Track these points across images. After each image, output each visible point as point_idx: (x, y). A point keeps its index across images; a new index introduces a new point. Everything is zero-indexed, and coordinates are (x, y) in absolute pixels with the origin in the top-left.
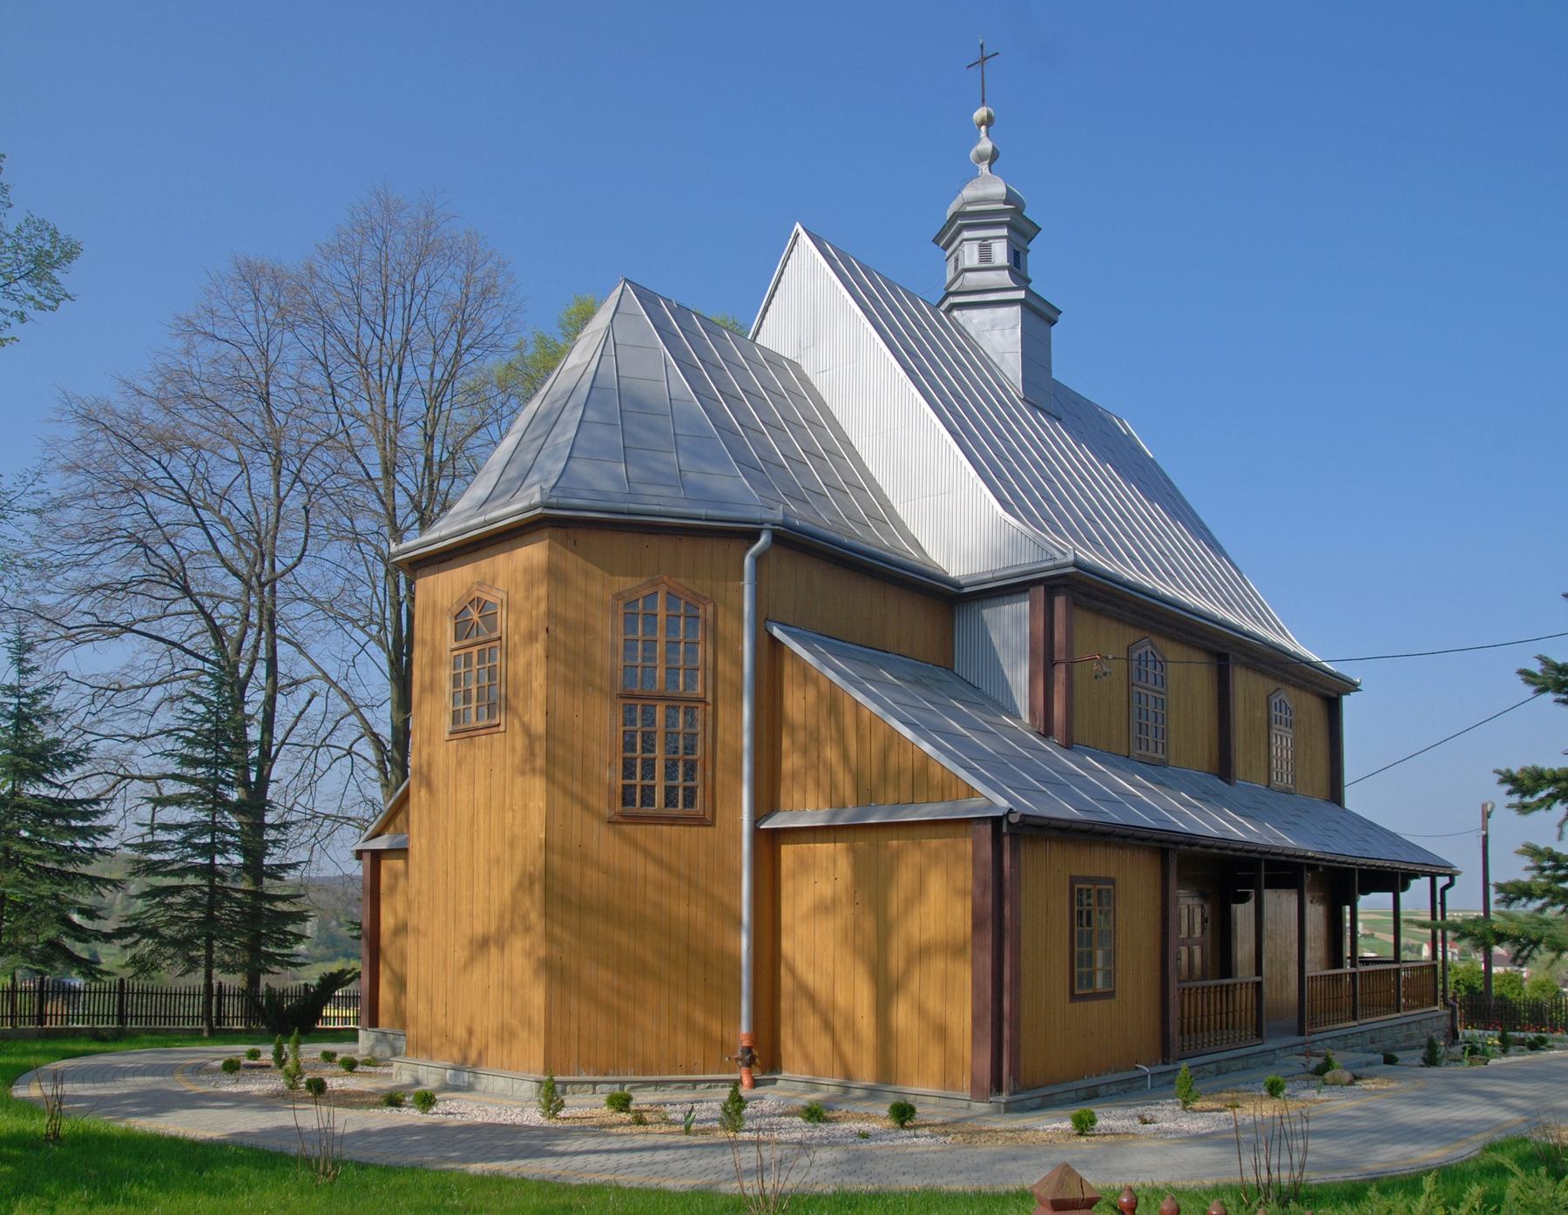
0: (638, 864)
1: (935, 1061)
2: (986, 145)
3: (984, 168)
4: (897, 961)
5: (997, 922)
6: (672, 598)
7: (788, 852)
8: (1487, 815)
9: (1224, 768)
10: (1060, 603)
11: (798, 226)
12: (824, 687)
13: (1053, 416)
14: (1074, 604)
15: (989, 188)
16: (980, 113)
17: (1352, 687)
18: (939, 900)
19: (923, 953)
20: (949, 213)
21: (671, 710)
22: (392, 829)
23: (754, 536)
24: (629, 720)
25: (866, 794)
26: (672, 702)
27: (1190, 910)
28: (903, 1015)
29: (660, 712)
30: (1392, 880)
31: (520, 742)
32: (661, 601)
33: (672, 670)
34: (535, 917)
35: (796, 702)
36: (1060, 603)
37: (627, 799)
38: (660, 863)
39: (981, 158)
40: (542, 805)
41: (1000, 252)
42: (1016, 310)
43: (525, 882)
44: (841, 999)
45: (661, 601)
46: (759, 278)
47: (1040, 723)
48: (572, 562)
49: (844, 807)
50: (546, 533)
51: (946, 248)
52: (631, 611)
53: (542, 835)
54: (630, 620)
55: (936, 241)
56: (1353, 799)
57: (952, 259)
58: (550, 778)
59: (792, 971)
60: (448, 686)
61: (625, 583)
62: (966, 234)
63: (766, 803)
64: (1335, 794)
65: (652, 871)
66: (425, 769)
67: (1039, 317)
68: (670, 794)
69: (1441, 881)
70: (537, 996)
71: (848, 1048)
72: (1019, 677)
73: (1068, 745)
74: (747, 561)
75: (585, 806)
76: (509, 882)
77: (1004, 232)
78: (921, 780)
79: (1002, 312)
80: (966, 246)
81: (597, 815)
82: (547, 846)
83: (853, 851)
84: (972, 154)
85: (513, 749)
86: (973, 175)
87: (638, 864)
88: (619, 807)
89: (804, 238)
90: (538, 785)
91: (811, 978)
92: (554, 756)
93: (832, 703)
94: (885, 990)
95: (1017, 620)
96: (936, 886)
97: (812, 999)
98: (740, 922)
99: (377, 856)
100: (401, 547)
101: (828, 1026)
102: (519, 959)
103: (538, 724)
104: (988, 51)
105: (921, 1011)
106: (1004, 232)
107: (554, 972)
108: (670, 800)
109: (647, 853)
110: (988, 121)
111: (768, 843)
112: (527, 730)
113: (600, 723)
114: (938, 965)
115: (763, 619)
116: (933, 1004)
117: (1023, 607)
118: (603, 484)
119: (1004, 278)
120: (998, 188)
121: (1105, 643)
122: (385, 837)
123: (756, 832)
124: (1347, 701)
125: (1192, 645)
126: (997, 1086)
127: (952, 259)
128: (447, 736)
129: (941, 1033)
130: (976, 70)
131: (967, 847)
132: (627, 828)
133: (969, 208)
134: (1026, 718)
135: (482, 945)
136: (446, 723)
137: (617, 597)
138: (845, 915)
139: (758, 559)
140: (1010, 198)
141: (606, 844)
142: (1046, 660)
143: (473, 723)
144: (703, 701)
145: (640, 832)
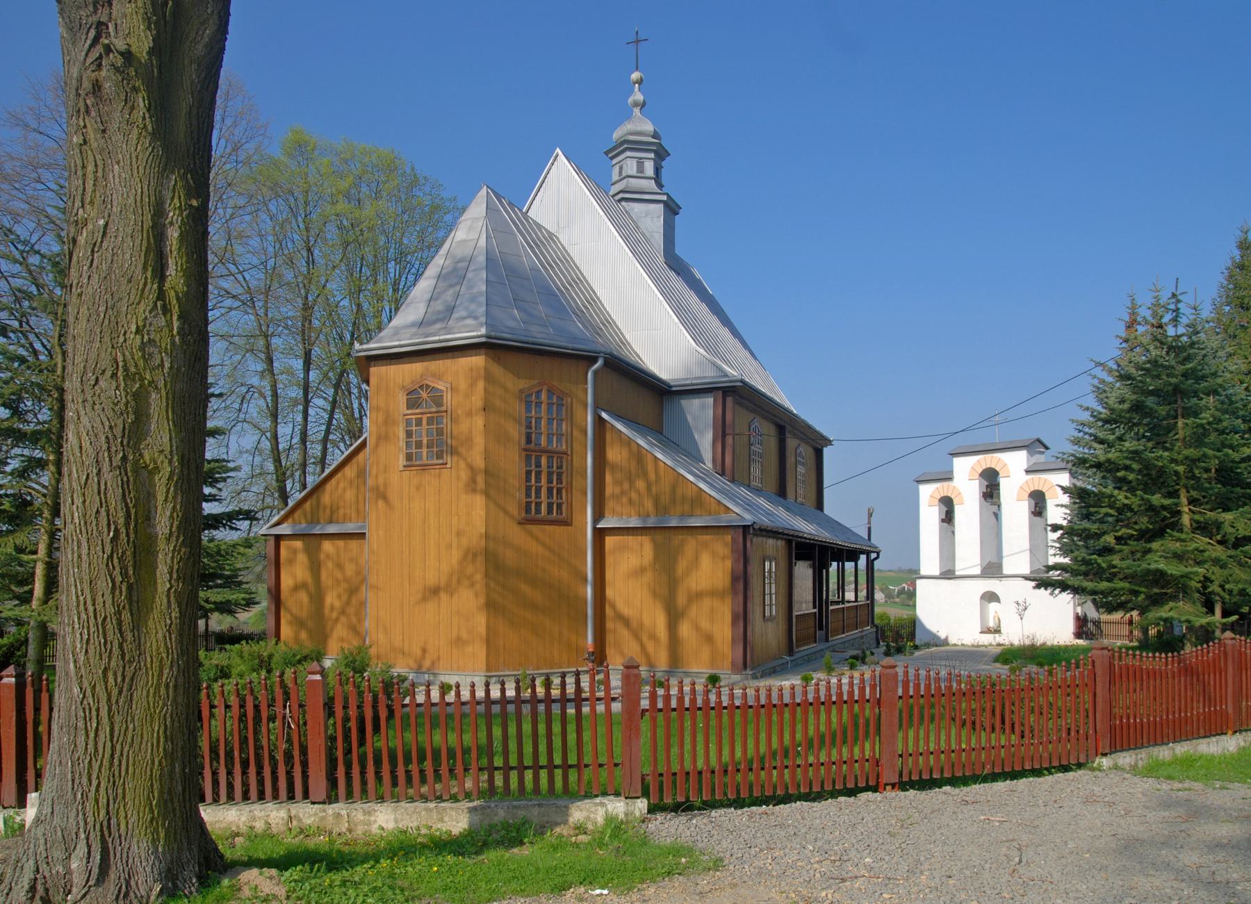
0: (534, 547)
1: (705, 654)
2: (638, 96)
3: (637, 111)
4: (681, 600)
5: (742, 581)
6: (550, 392)
7: (610, 541)
8: (870, 515)
9: (782, 492)
10: (729, 401)
11: (558, 150)
12: (634, 447)
13: (678, 274)
14: (736, 402)
15: (641, 125)
16: (635, 76)
17: (828, 442)
18: (709, 568)
19: (697, 596)
20: (617, 135)
21: (550, 458)
22: (290, 520)
23: (595, 360)
24: (528, 462)
25: (661, 509)
26: (550, 454)
27: (804, 572)
28: (685, 630)
29: (544, 461)
30: (853, 555)
31: (464, 475)
32: (544, 396)
33: (550, 436)
34: (479, 577)
35: (614, 454)
36: (729, 401)
37: (528, 510)
38: (544, 545)
39: (636, 104)
40: (483, 513)
41: (649, 168)
42: (661, 206)
43: (469, 555)
44: (647, 621)
45: (544, 396)
46: (530, 177)
47: (719, 468)
48: (497, 371)
49: (648, 516)
50: (483, 351)
51: (612, 158)
52: (528, 399)
53: (483, 531)
54: (528, 405)
55: (607, 153)
56: (828, 510)
57: (617, 167)
58: (487, 494)
59: (613, 606)
60: (402, 435)
61: (523, 384)
62: (628, 154)
63: (598, 515)
64: (820, 505)
65: (541, 549)
66: (382, 488)
67: (671, 209)
68: (550, 506)
69: (873, 556)
70: (481, 621)
71: (650, 647)
72: (705, 441)
73: (733, 481)
74: (590, 375)
75: (506, 512)
76: (456, 555)
77: (652, 156)
78: (698, 500)
79: (652, 206)
80: (629, 161)
81: (512, 517)
82: (487, 536)
83: (654, 541)
84: (630, 100)
85: (458, 478)
86: (629, 117)
87: (534, 547)
88: (523, 515)
89: (562, 158)
90: (480, 500)
91: (625, 611)
92: (488, 481)
93: (639, 456)
94: (674, 617)
95: (703, 407)
96: (706, 560)
97: (626, 622)
98: (586, 580)
99: (278, 538)
100: (365, 347)
101: (637, 637)
102: (469, 600)
103: (480, 463)
104: (641, 37)
105: (697, 628)
106: (652, 156)
107: (491, 606)
108: (550, 511)
109: (538, 540)
110: (640, 82)
111: (600, 534)
112: (471, 467)
113: (512, 463)
114: (707, 603)
115: (597, 407)
116: (705, 624)
117: (709, 401)
118: (514, 324)
119: (652, 185)
120: (649, 127)
121: (741, 419)
122: (285, 525)
123: (595, 529)
124: (827, 452)
125: (765, 418)
126: (745, 667)
127: (617, 167)
128: (401, 468)
129: (709, 639)
130: (633, 46)
131: (729, 538)
132: (529, 527)
133: (631, 138)
134: (709, 464)
135: (434, 591)
136: (402, 461)
137: (521, 391)
138: (648, 577)
139: (596, 373)
140: (655, 135)
141: (517, 535)
142: (722, 431)
143: (425, 461)
144: (566, 453)
145: (534, 528)
